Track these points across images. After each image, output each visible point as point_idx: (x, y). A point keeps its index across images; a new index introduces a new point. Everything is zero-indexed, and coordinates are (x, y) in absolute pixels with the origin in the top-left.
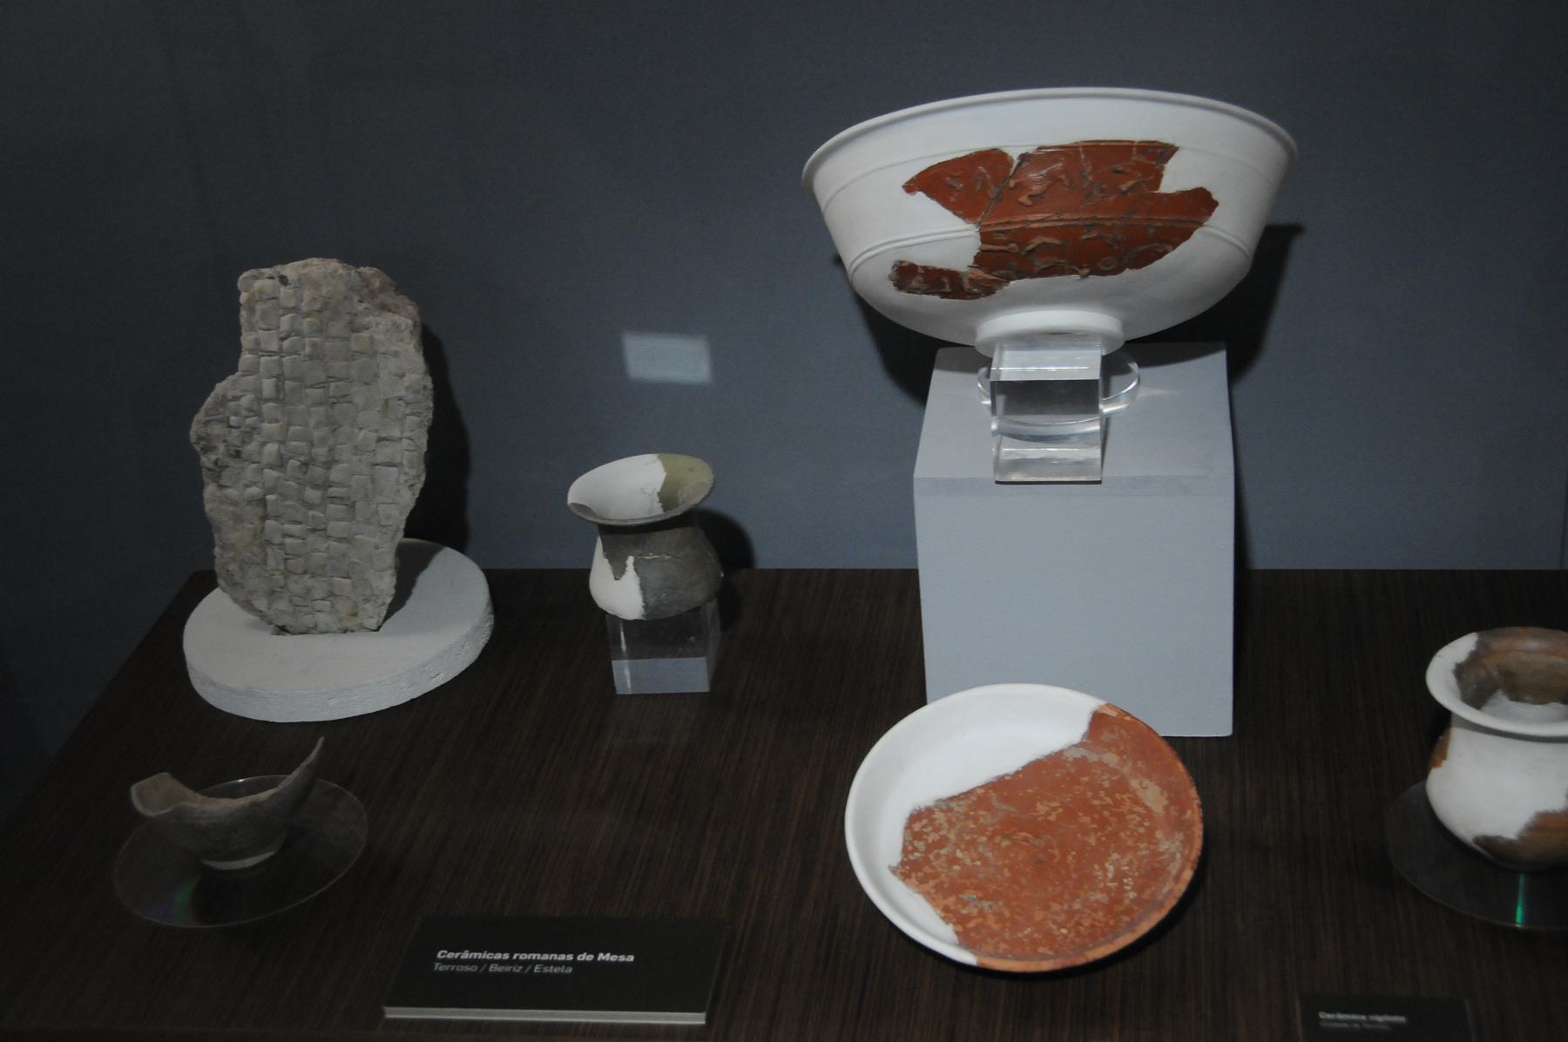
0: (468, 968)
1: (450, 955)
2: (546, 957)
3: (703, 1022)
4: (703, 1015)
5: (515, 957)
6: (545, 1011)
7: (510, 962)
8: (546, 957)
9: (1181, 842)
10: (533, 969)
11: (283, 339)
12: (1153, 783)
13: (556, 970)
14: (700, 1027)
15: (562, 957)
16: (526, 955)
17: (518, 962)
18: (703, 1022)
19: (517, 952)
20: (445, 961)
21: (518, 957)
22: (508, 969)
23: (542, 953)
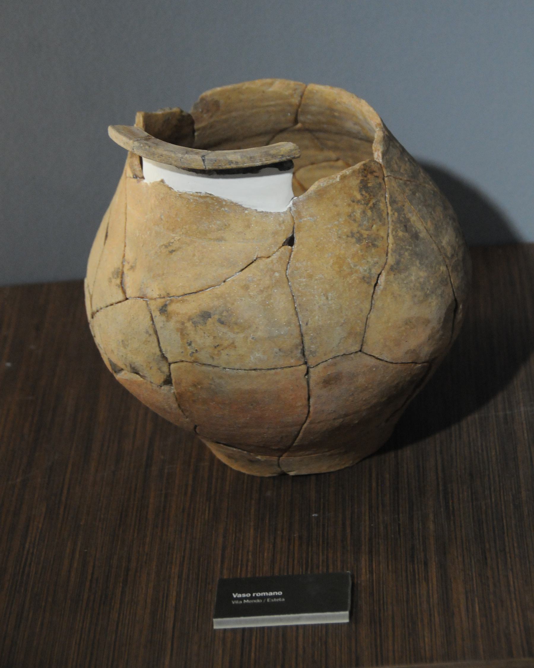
0: (258, 601)
1: (240, 596)
2: (271, 594)
3: (347, 620)
4: (347, 613)
5: (254, 595)
6: (272, 617)
7: (251, 598)
8: (271, 594)
9: (401, 274)
10: (266, 600)
11: (238, 382)
12: (380, 206)
13: (277, 600)
14: (348, 623)
15: (244, 595)
16: (260, 594)
17: (256, 598)
18: (347, 620)
19: (254, 593)
20: (237, 599)
21: (255, 595)
22: (252, 601)
23: (241, 593)
